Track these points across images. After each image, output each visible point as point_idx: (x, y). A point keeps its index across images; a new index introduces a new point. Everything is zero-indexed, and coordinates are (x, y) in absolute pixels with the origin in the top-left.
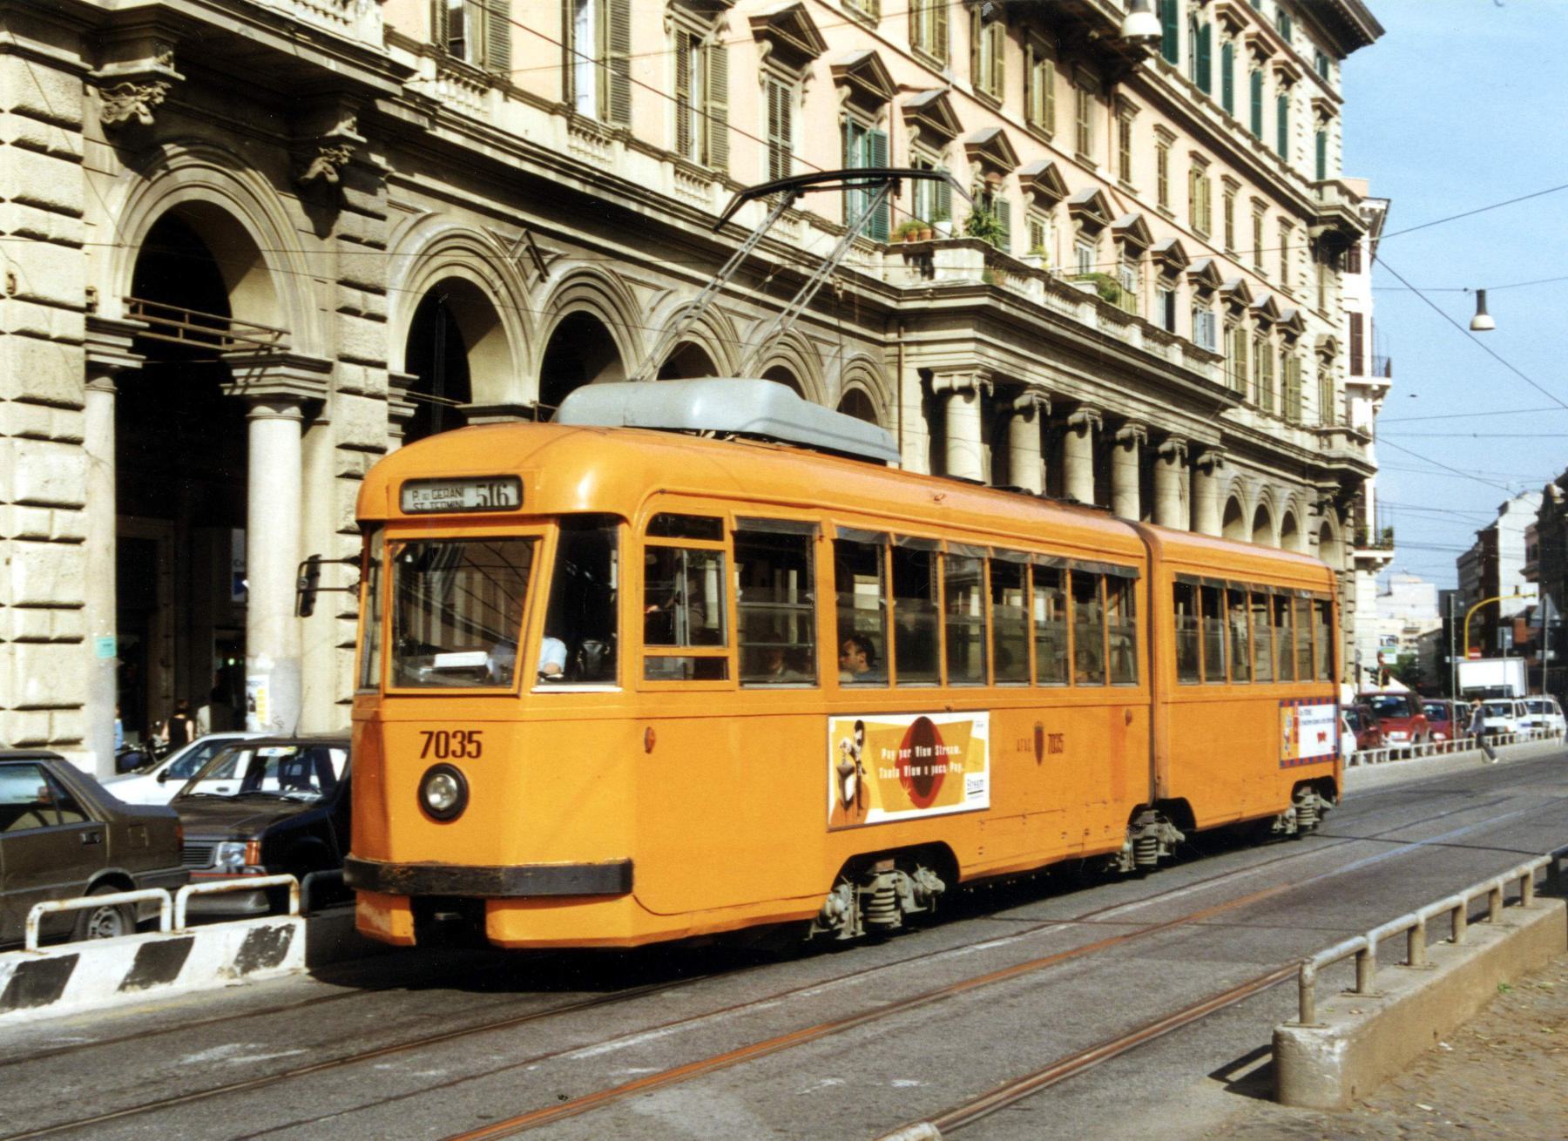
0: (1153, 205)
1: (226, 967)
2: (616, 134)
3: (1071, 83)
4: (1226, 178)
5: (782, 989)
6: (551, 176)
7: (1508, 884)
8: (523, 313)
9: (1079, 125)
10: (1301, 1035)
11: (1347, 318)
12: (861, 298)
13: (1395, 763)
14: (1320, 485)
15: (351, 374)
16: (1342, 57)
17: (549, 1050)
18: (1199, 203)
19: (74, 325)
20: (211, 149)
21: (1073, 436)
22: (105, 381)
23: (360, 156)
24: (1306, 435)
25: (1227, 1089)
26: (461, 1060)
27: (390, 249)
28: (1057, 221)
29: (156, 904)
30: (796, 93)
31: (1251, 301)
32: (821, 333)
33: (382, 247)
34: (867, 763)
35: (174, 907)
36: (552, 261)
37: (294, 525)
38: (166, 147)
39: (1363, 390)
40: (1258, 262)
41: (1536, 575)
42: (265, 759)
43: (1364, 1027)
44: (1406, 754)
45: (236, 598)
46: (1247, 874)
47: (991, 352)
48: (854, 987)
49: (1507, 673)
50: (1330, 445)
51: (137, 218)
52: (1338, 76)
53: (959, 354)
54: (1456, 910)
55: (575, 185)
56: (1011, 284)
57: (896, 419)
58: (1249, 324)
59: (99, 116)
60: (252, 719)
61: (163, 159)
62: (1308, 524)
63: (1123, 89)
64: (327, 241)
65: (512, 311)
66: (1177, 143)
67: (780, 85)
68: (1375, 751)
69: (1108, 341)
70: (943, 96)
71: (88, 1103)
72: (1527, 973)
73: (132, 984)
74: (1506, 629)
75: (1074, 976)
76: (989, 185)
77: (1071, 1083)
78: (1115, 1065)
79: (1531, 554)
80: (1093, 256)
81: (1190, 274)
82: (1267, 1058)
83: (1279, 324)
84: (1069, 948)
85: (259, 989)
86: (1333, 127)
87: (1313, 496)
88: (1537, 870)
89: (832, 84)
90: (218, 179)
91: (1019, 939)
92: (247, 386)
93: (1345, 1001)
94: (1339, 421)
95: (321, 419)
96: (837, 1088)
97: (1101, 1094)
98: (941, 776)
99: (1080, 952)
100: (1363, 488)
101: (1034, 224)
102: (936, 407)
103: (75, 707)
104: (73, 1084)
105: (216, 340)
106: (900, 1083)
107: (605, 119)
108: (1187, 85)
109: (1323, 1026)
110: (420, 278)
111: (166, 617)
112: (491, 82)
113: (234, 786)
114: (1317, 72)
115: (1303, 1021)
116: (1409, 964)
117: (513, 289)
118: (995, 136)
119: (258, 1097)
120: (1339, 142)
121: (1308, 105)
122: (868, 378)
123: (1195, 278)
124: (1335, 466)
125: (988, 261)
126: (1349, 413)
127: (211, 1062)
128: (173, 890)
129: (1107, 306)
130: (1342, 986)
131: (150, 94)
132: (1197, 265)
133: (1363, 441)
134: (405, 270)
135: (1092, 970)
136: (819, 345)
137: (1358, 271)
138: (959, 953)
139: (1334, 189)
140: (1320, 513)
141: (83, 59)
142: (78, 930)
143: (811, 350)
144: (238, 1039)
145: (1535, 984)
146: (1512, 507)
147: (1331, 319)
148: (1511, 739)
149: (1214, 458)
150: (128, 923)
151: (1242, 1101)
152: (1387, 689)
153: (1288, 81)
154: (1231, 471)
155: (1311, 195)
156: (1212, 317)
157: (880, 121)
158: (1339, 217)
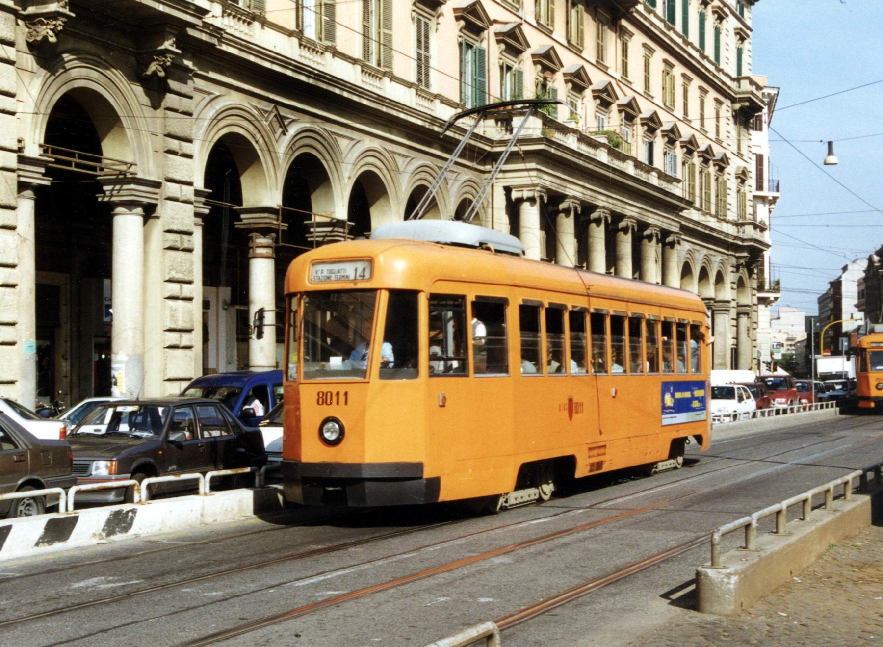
0: (641, 91)
1: (97, 533)
2: (327, 49)
3: (594, 19)
4: (684, 75)
5: (417, 545)
6: (289, 73)
7: (836, 487)
9: (598, 44)
10: (711, 573)
11: (754, 157)
13: (779, 416)
14: (737, 254)
15: (172, 189)
16: (752, 4)
17: (282, 581)
18: (668, 89)
19: (11, 160)
20: (90, 57)
21: (593, 225)
22: (29, 193)
23: (178, 62)
24: (730, 225)
25: (670, 604)
26: (230, 587)
27: (195, 116)
29: (57, 497)
30: (432, 24)
31: (698, 147)
33: (190, 115)
35: (67, 499)
36: (290, 123)
37: (139, 277)
38: (64, 56)
39: (763, 199)
40: (702, 124)
41: (864, 307)
42: (121, 413)
43: (748, 569)
44: (785, 412)
45: (106, 319)
47: (546, 177)
48: (459, 545)
51: (47, 97)
52: (750, 15)
53: (528, 178)
54: (805, 501)
55: (303, 78)
56: (557, 137)
57: (490, 216)
58: (697, 160)
59: (25, 37)
60: (114, 389)
61: (62, 62)
62: (730, 277)
63: (624, 22)
64: (158, 111)
65: (266, 153)
66: (655, 54)
67: (423, 20)
68: (767, 410)
69: (614, 170)
70: (519, 26)
71: (16, 610)
72: (847, 537)
73: (43, 542)
74: (844, 339)
75: (585, 539)
76: (545, 79)
77: (581, 600)
78: (606, 590)
79: (861, 295)
80: (606, 121)
81: (662, 131)
82: (693, 587)
83: (714, 161)
84: (584, 523)
85: (116, 546)
86: (747, 45)
87: (734, 261)
88: (854, 478)
89: (454, 19)
90: (94, 74)
92: (112, 196)
93: (738, 553)
94: (749, 217)
95: (155, 215)
96: (447, 602)
97: (597, 607)
99: (592, 525)
100: (763, 257)
102: (513, 209)
103: (12, 382)
104: (7, 600)
105: (94, 169)
106: (482, 600)
107: (320, 39)
108: (662, 21)
109: (724, 567)
110: (212, 133)
111: (65, 330)
112: (254, 18)
113: (103, 429)
114: (738, 13)
116: (776, 532)
117: (267, 139)
118: (549, 50)
119: (114, 607)
121: (732, 32)
123: (665, 134)
125: (544, 124)
126: (755, 212)
127: (88, 587)
128: (67, 489)
129: (613, 152)
130: (739, 545)
131: (55, 25)
132: (666, 127)
133: (763, 229)
135: (596, 536)
137: (761, 130)
139: (747, 82)
140: (738, 271)
141: (15, 4)
142: (12, 510)
144: (103, 574)
146: (849, 267)
147: (744, 158)
149: (676, 239)
150: (41, 508)
151: (678, 610)
152: (775, 374)
153: (721, 18)
154: (686, 246)
156: (675, 156)
157: (481, 41)
158: (750, 98)
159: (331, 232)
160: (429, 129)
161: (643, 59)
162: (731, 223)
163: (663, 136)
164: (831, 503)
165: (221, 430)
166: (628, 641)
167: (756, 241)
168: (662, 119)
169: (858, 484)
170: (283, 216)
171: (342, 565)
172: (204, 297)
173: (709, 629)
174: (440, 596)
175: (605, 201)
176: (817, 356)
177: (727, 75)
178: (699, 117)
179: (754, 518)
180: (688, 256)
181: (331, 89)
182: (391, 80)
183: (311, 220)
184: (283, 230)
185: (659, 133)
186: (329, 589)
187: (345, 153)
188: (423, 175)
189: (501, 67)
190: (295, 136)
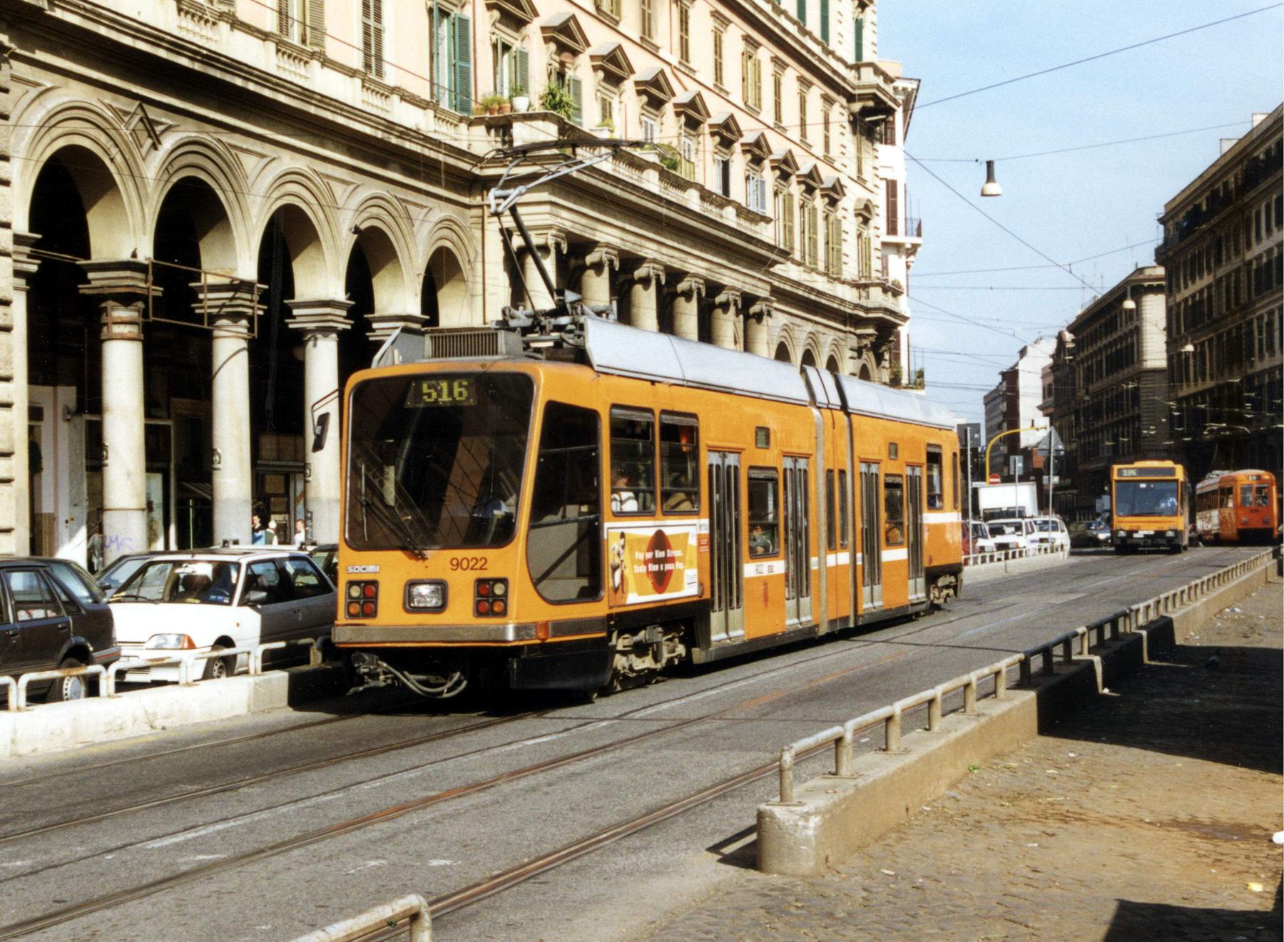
0: (710, 83)
2: (222, 16)
6: (162, 53)
8: (138, 180)
9: (644, 11)
10: (780, 812)
11: (883, 185)
12: (447, 165)
14: (859, 331)
17: (128, 841)
18: (751, 81)
21: (638, 288)
24: (847, 288)
25: (720, 861)
26: (46, 852)
28: (624, 97)
31: (798, 169)
32: (412, 196)
34: (627, 562)
39: (898, 247)
40: (804, 134)
41: (1051, 410)
43: (835, 805)
46: (773, 674)
47: (564, 214)
49: (1021, 496)
50: (868, 297)
53: (546, 217)
54: (931, 702)
55: (184, 62)
58: (796, 189)
69: (669, 204)
72: (997, 755)
75: (606, 766)
76: (562, 64)
78: (626, 843)
79: (1047, 391)
80: (656, 128)
81: (743, 145)
83: (822, 189)
86: (869, 15)
87: (853, 342)
91: (565, 735)
96: (379, 868)
98: (670, 572)
100: (898, 335)
101: (604, 100)
102: (514, 264)
106: (435, 863)
109: (800, 804)
115: (783, 799)
116: (886, 750)
118: (568, 20)
120: (875, 29)
122: (455, 238)
124: (871, 315)
126: (885, 269)
129: (669, 174)
132: (749, 138)
133: (896, 293)
134: (27, 139)
136: (410, 207)
137: (893, 143)
138: (508, 748)
139: (871, 70)
140: (860, 356)
143: (403, 214)
145: (1002, 764)
146: (1030, 350)
147: (867, 185)
148: (1021, 553)
149: (764, 308)
151: (732, 871)
155: (850, 75)
156: (763, 183)
158: (875, 95)
159: (231, 299)
160: (381, 140)
161: (712, 36)
162: (849, 284)
163: (745, 152)
164: (973, 705)
165: (46, 609)
166: (649, 918)
167: (887, 310)
168: (742, 127)
169: (1017, 676)
170: (154, 274)
171: (225, 814)
172: (30, 402)
173: (776, 897)
174: (371, 859)
175: (657, 251)
176: (976, 484)
177: (840, 60)
178: (798, 122)
179: (848, 730)
180: (784, 333)
181: (228, 78)
182: (323, 65)
183: (199, 280)
184: (155, 298)
185: (737, 147)
186: (200, 852)
187: (251, 179)
188: (375, 211)
189: (495, 46)
190: (173, 151)
